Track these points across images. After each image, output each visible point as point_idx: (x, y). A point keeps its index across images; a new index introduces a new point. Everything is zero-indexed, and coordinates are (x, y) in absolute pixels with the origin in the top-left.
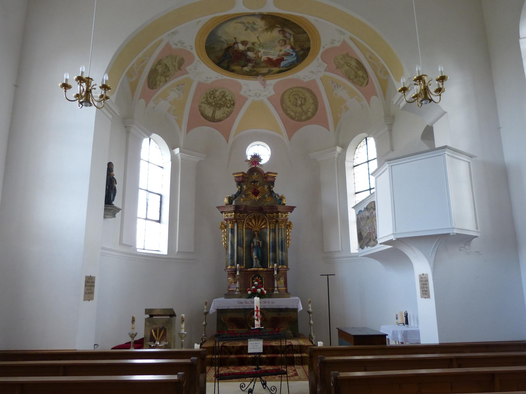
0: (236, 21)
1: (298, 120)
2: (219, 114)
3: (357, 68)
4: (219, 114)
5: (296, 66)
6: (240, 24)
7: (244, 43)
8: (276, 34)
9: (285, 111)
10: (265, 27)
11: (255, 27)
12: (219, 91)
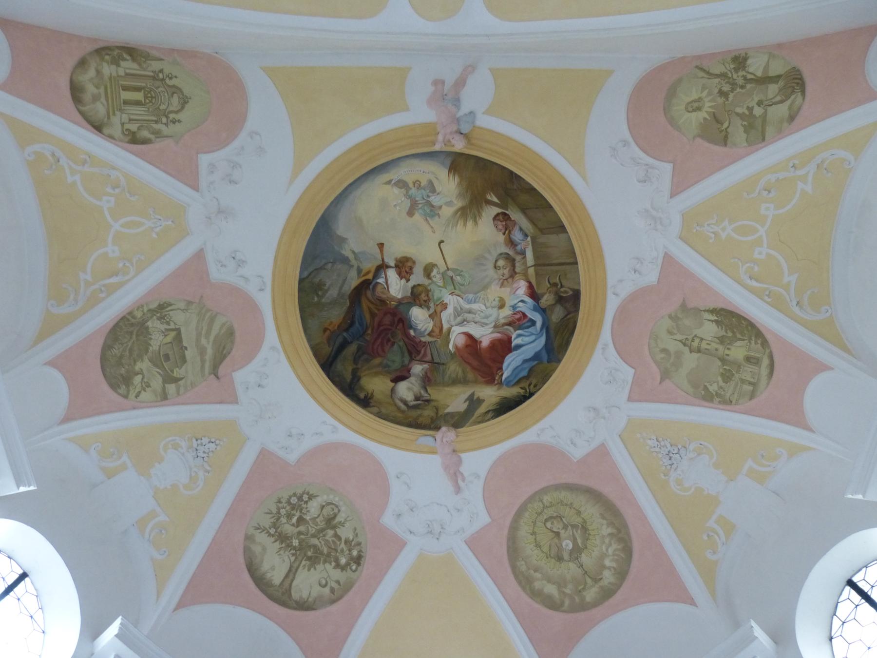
0: (385, 177)
1: (573, 609)
2: (307, 583)
3: (722, 340)
4: (307, 583)
5: (546, 377)
6: (396, 190)
7: (404, 267)
8: (484, 231)
9: (525, 582)
10: (459, 204)
11: (435, 200)
12: (319, 499)
